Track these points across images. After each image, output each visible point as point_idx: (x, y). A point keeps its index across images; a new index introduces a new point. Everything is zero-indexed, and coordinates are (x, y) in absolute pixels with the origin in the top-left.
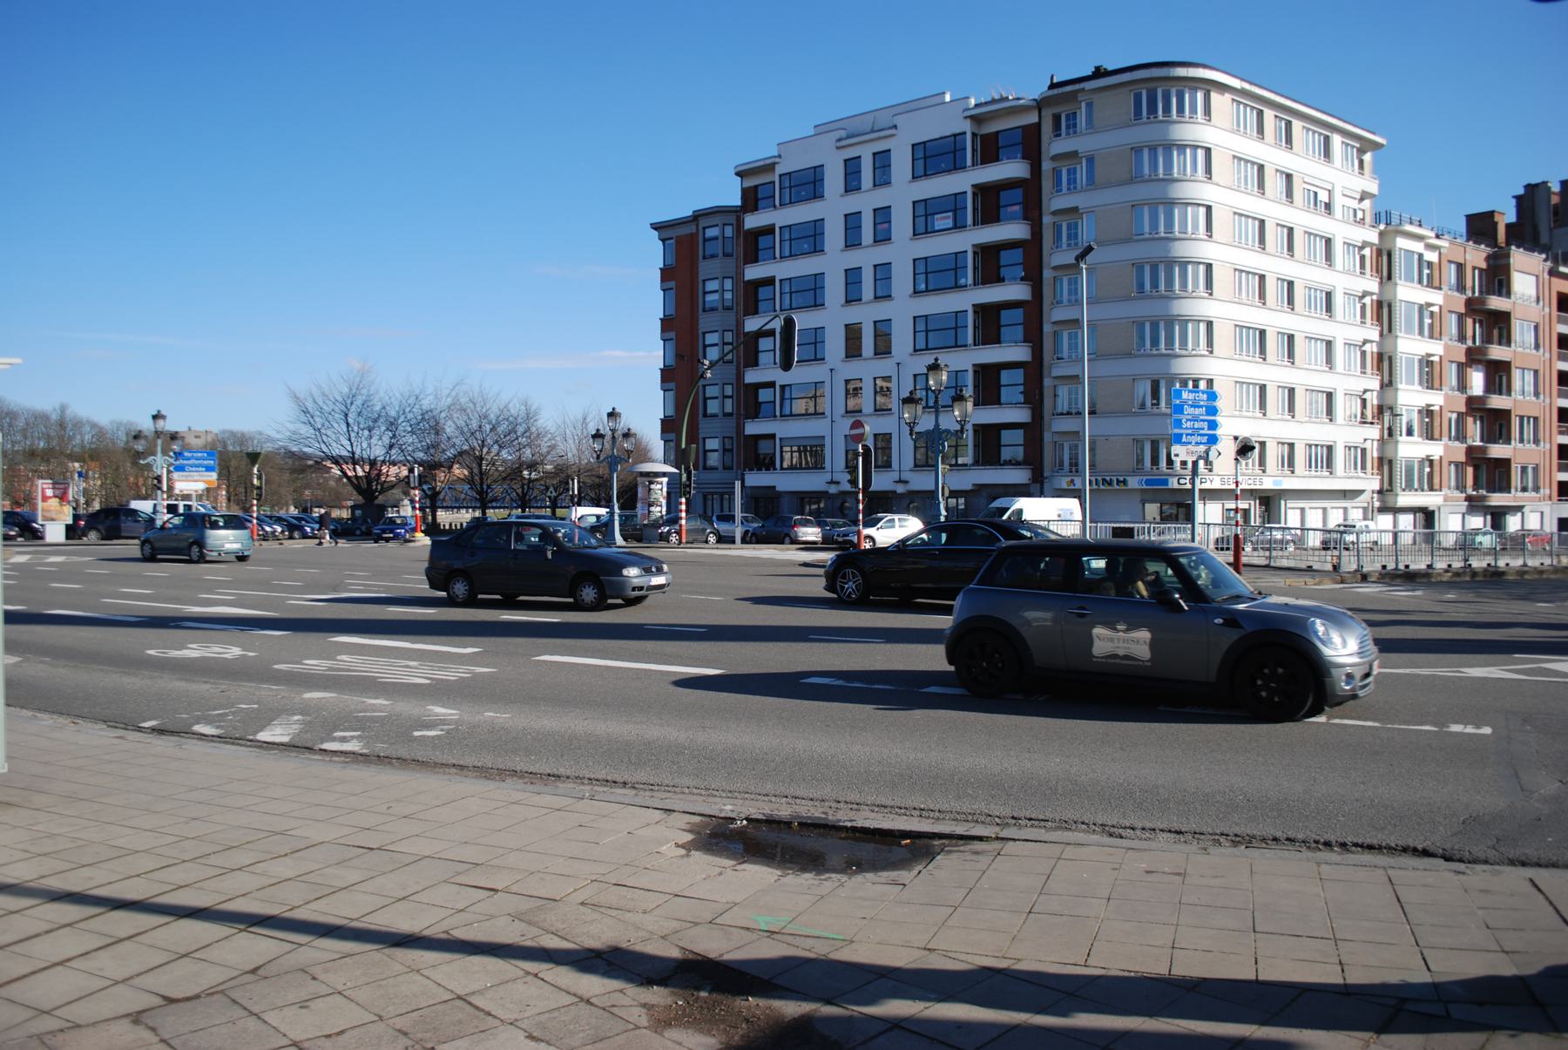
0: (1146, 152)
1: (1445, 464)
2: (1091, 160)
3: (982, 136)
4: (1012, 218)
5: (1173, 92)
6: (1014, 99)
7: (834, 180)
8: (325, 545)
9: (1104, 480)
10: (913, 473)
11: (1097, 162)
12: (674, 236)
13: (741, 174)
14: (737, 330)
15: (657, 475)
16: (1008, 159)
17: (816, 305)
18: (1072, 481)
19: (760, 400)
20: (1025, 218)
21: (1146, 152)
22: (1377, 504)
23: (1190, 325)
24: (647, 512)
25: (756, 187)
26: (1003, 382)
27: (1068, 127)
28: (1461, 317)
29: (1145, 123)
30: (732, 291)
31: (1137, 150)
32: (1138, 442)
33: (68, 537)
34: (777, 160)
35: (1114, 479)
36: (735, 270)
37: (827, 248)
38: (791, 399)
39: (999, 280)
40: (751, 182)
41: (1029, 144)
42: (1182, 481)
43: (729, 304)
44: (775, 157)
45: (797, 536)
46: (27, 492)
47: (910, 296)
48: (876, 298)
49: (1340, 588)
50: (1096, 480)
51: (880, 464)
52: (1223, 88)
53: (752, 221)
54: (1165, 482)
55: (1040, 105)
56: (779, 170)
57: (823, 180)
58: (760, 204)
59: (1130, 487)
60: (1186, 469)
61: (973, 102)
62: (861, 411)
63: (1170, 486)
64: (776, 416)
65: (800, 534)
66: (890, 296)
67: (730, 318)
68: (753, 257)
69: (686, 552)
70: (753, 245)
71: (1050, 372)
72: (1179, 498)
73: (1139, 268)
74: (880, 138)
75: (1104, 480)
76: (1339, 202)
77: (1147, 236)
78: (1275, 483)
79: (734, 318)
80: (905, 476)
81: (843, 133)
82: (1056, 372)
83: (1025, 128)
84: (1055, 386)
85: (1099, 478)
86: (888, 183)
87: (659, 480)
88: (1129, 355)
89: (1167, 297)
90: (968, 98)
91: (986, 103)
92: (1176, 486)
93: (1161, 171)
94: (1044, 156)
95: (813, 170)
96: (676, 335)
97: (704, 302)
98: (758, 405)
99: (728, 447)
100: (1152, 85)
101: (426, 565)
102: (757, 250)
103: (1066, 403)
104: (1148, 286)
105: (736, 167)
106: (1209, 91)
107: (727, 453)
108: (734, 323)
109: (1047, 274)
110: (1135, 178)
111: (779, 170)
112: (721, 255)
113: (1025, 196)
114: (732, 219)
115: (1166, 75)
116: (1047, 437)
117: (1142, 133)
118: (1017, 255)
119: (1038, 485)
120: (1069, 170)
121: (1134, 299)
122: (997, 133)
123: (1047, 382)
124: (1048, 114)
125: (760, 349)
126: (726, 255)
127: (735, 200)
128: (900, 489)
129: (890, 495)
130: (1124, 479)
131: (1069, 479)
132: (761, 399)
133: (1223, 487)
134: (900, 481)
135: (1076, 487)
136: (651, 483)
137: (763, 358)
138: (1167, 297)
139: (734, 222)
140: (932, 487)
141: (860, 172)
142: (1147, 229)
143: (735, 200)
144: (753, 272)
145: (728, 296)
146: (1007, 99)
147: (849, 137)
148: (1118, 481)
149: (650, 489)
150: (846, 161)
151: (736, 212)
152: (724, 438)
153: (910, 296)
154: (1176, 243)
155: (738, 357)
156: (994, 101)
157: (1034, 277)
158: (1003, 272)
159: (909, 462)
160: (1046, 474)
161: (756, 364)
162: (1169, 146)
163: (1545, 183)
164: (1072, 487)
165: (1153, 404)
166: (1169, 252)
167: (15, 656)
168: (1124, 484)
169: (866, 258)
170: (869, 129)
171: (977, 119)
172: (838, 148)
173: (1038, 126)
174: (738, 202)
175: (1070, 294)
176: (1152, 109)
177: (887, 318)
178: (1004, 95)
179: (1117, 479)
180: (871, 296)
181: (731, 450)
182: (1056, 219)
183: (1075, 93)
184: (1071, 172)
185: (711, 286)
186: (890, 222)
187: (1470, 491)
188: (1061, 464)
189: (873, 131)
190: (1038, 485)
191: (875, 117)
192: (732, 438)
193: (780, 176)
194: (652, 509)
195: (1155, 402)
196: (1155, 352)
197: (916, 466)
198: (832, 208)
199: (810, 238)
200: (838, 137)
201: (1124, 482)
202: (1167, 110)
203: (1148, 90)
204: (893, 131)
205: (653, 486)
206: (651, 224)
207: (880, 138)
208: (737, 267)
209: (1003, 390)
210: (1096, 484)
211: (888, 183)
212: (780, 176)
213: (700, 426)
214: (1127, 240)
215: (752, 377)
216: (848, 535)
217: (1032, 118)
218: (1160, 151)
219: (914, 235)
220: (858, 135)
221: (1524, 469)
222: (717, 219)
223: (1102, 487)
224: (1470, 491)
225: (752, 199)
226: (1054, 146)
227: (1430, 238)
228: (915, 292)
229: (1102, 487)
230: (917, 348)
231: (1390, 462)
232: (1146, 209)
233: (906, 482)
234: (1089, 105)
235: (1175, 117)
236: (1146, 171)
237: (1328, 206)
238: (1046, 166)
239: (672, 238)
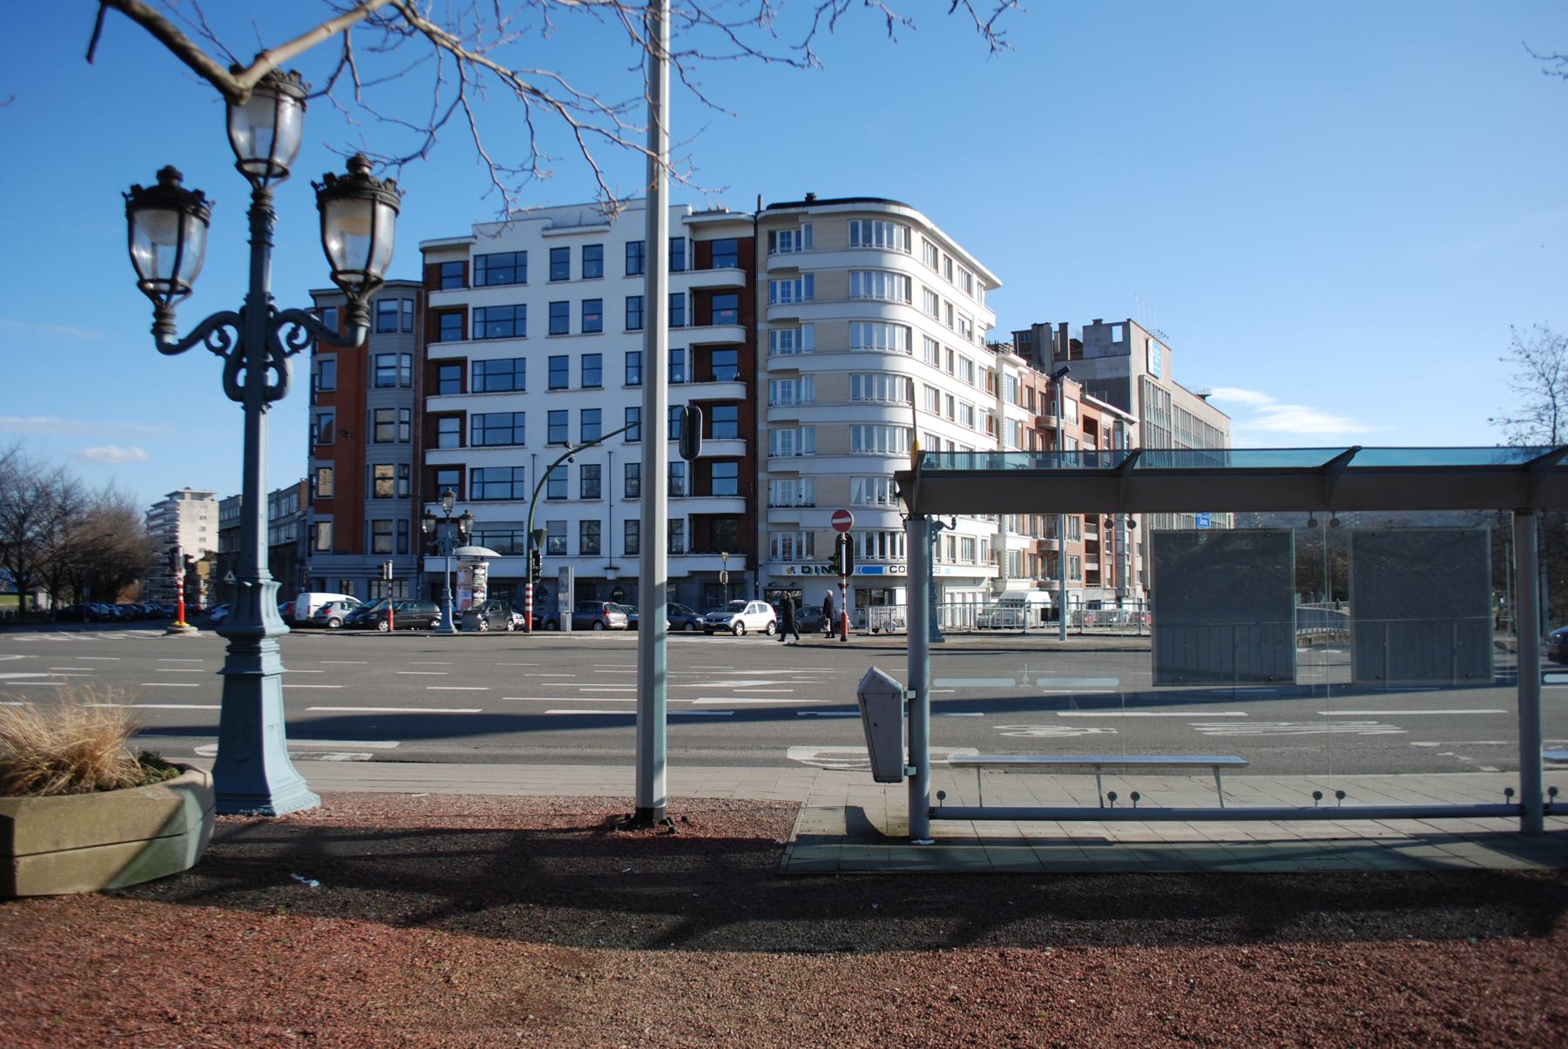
0: (862, 276)
1: (1026, 555)
2: (810, 277)
3: (696, 243)
4: (724, 322)
5: (885, 225)
6: (731, 213)
7: (538, 267)
9: (823, 568)
10: (624, 560)
11: (816, 279)
12: (337, 305)
13: (424, 251)
14: (415, 408)
15: (483, 559)
16: (721, 267)
17: (514, 390)
18: (792, 569)
19: (440, 482)
20: (739, 323)
21: (862, 276)
22: (991, 590)
23: (897, 431)
24: (470, 598)
25: (440, 265)
26: (715, 474)
27: (782, 245)
28: (1032, 432)
29: (860, 250)
30: (410, 368)
31: (854, 273)
33: (636, 629)
34: (473, 240)
36: (413, 347)
37: (528, 333)
38: (484, 483)
39: (712, 379)
40: (433, 259)
41: (745, 255)
42: (893, 569)
43: (406, 382)
44: (470, 237)
45: (608, 621)
47: (623, 388)
48: (583, 387)
51: (585, 550)
52: (919, 225)
53: (438, 299)
54: (880, 570)
55: (756, 221)
56: (474, 251)
57: (525, 266)
58: (445, 282)
61: (690, 210)
62: (566, 498)
63: (884, 574)
64: (465, 500)
65: (612, 620)
66: (600, 386)
67: (408, 397)
68: (435, 336)
70: (436, 324)
71: (766, 468)
72: (885, 584)
73: (855, 377)
74: (592, 232)
75: (823, 568)
76: (978, 333)
77: (863, 350)
78: (948, 571)
79: (412, 397)
80: (615, 563)
81: (548, 223)
82: (773, 467)
83: (741, 240)
84: (769, 481)
85: (819, 566)
86: (599, 275)
87: (483, 564)
88: (847, 455)
89: (881, 405)
90: (686, 205)
91: (702, 213)
92: (889, 574)
93: (874, 293)
94: (760, 268)
95: (513, 255)
96: (337, 410)
97: (377, 377)
98: (438, 487)
99: (403, 530)
100: (868, 217)
101: (221, 664)
102: (440, 329)
103: (779, 495)
104: (863, 395)
105: (424, 242)
106: (909, 228)
107: (401, 537)
108: (412, 402)
109: (762, 376)
110: (852, 298)
111: (474, 251)
112: (399, 330)
113: (740, 301)
114: (413, 294)
115: (882, 210)
116: (762, 527)
117: (857, 259)
118: (732, 357)
119: (753, 572)
120: (783, 284)
121: (851, 405)
122: (712, 241)
123: (761, 476)
124: (763, 231)
125: (441, 430)
126: (405, 331)
127: (416, 275)
128: (611, 575)
129: (594, 582)
131: (789, 567)
132: (441, 482)
134: (611, 568)
135: (796, 574)
136: (475, 567)
137: (443, 440)
138: (881, 405)
139: (415, 298)
140: (444, 570)
141: (568, 262)
142: (862, 344)
143: (416, 275)
144: (437, 351)
145: (406, 373)
146: (723, 212)
147: (555, 227)
149: (474, 574)
150: (552, 250)
151: (417, 287)
152: (399, 520)
153: (623, 388)
154: (889, 358)
155: (416, 438)
156: (709, 212)
157: (748, 376)
158: (715, 371)
159: (619, 548)
160: (760, 563)
161: (437, 446)
162: (883, 272)
163: (1048, 324)
164: (792, 574)
166: (882, 365)
167: (813, 747)
169: (575, 347)
170: (576, 223)
171: (694, 227)
172: (544, 236)
173: (754, 240)
174: (419, 278)
175: (783, 395)
176: (867, 239)
178: (721, 208)
180: (579, 385)
181: (406, 534)
182: (771, 326)
183: (797, 215)
184: (786, 286)
185: (385, 361)
186: (601, 314)
187: (1040, 579)
188: (775, 552)
189: (580, 225)
190: (753, 572)
191: (582, 212)
192: (407, 521)
193: (475, 257)
194: (476, 595)
196: (870, 453)
197: (626, 553)
198: (536, 294)
199: (511, 322)
200: (544, 225)
202: (880, 241)
203: (864, 221)
204: (607, 227)
205: (477, 571)
206: (310, 291)
207: (592, 232)
208: (416, 344)
209: (715, 482)
211: (599, 275)
212: (475, 257)
214: (846, 352)
215: (433, 458)
216: (722, 620)
217: (748, 232)
218: (874, 276)
219: (627, 329)
220: (569, 227)
221: (1071, 559)
222: (396, 293)
223: (822, 574)
224: (1040, 579)
225: (434, 277)
226: (771, 261)
227: (1022, 365)
228: (627, 384)
229: (822, 574)
230: (629, 438)
231: (999, 553)
232: (862, 326)
233: (616, 569)
234: (809, 228)
235: (874, 247)
236: (862, 292)
237: (970, 334)
238: (762, 277)
239: (334, 308)
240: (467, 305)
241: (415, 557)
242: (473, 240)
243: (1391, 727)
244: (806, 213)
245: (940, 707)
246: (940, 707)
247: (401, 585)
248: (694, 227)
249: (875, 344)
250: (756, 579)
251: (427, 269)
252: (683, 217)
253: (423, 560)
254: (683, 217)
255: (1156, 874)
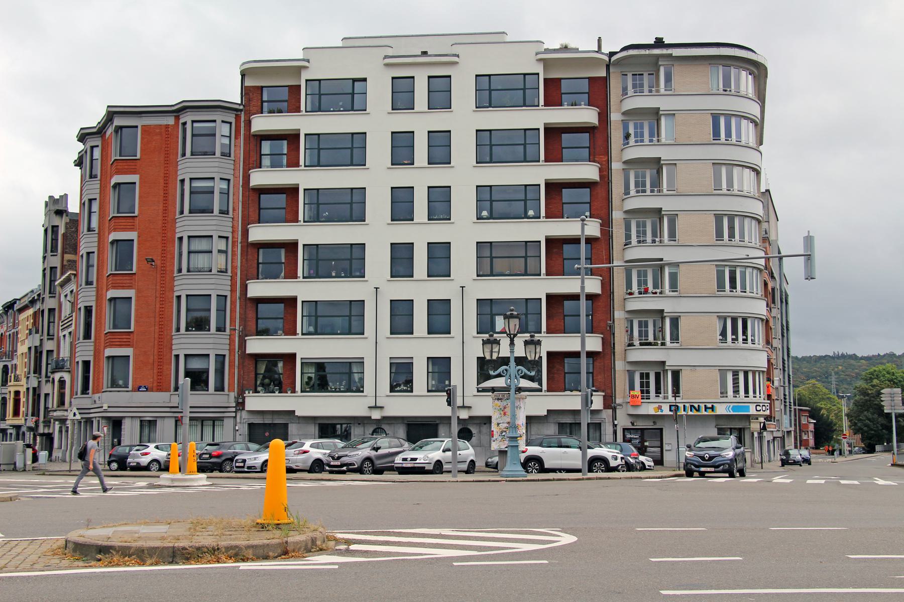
8: (83, 495)
18: (660, 408)
32: (723, 372)
35: (702, 406)
46: (5, 352)
49: (27, 501)
50: (684, 406)
53: (261, 123)
59: (718, 413)
60: (748, 397)
69: (674, 482)
111: (305, 76)
127: (234, 96)
130: (713, 406)
133: (656, 414)
139: (233, 120)
143: (234, 96)
148: (706, 408)
155: (234, 268)
160: (618, 401)
165: (733, 339)
168: (713, 411)
171: (546, 63)
172: (458, 56)
177: (363, 243)
179: (705, 406)
195: (734, 337)
201: (712, 408)
204: (455, 59)
210: (684, 411)
213: (174, 342)
240: (299, 130)
241: (233, 395)
242: (306, 64)
243: (174, 386)
244: (670, 56)
245: (213, 440)
246: (213, 440)
247: (202, 425)
248: (546, 63)
249: (736, 187)
250: (614, 418)
251: (246, 91)
252: (537, 54)
253: (244, 398)
254: (537, 54)
255: (315, 551)
